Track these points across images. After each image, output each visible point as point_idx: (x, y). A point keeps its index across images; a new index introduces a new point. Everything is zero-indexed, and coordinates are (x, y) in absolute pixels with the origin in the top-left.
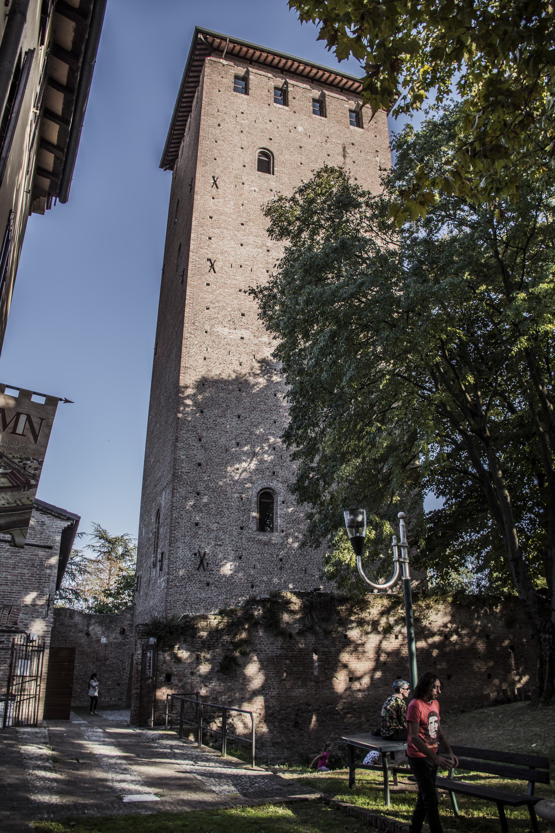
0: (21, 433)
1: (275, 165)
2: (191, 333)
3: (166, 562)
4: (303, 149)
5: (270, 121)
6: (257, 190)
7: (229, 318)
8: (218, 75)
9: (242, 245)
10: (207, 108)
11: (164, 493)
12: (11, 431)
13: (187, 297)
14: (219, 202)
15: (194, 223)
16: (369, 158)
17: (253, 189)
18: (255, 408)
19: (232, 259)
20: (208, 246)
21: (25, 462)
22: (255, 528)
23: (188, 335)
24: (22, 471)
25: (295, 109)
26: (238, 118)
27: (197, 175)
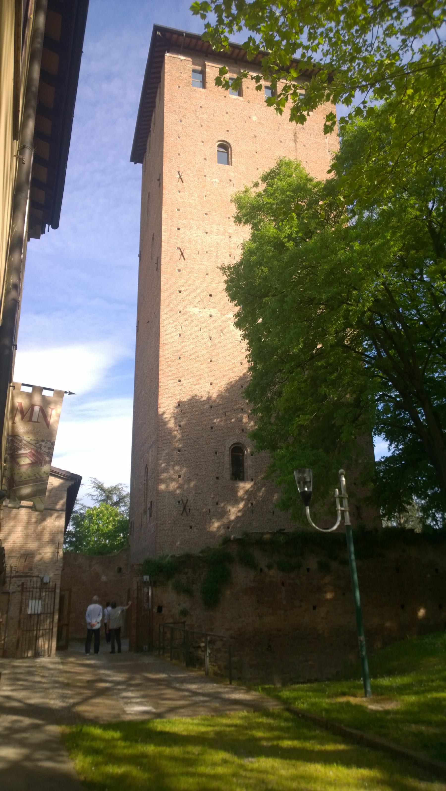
0: (36, 421)
1: (233, 156)
2: (167, 314)
3: (154, 509)
4: (257, 138)
5: (227, 113)
6: (218, 181)
7: (199, 300)
8: (177, 66)
9: (207, 233)
10: (169, 105)
11: (150, 451)
12: (28, 419)
13: (162, 283)
14: (185, 195)
15: (164, 216)
16: (318, 140)
17: (214, 180)
18: (224, 376)
19: (199, 246)
20: (178, 236)
21: (40, 443)
22: (229, 478)
23: (165, 316)
24: (39, 451)
25: (248, 99)
26: (198, 113)
27: (164, 171)
